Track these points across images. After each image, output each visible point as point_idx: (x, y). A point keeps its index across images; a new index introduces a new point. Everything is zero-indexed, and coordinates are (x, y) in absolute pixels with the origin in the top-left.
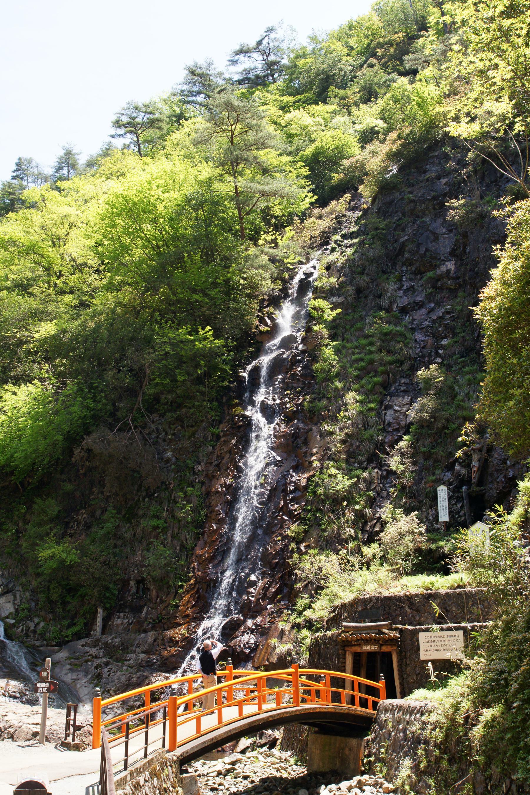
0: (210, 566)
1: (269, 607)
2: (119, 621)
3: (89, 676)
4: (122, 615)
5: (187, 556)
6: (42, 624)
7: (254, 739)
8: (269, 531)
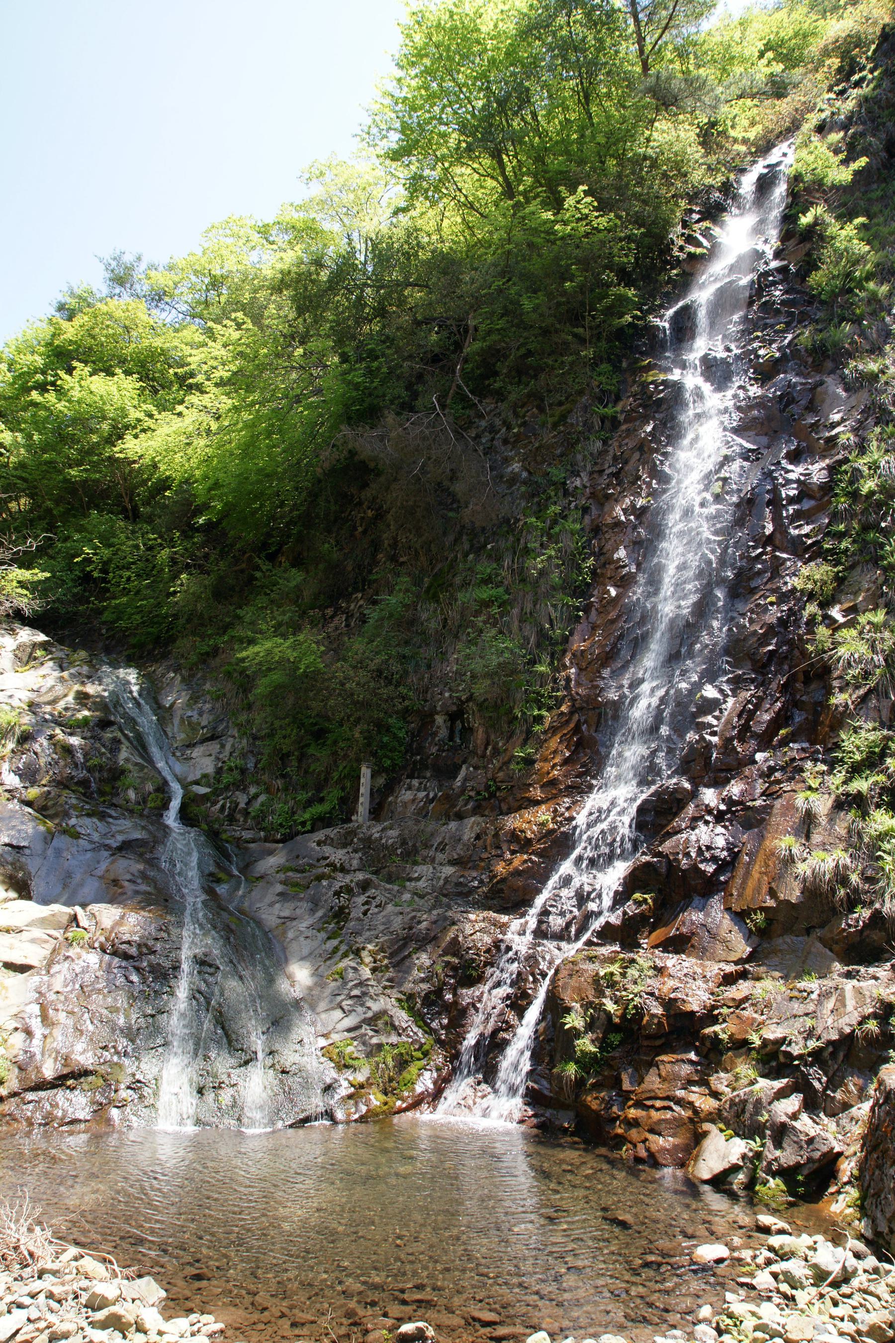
0: (606, 673)
1: (759, 756)
2: (407, 796)
3: (320, 913)
4: (415, 782)
5: (552, 656)
6: (262, 798)
7: (755, 1145)
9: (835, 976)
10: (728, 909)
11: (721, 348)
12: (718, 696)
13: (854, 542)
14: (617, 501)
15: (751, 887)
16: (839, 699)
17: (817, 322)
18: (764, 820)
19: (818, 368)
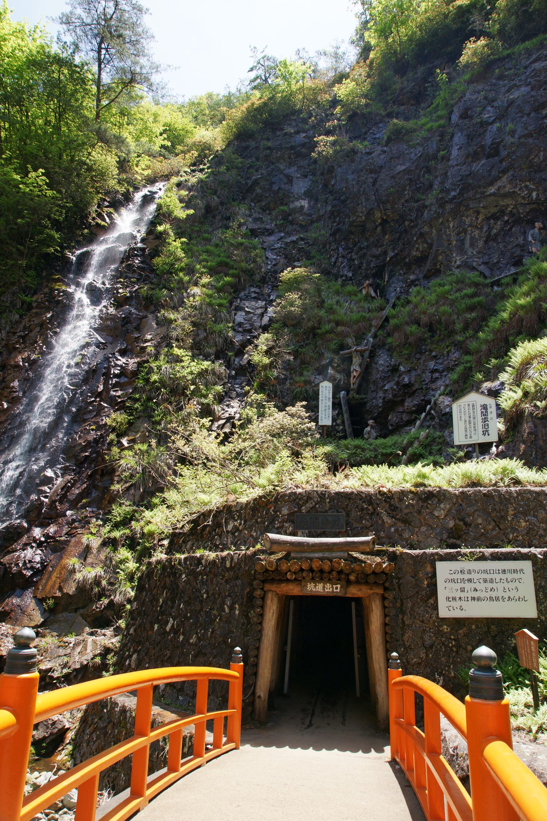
1: (69, 513)
8: (78, 419)
9: (85, 634)
10: (35, 597)
11: (100, 282)
12: (53, 476)
13: (142, 405)
14: (20, 352)
15: (50, 586)
16: (116, 487)
17: (152, 283)
18: (64, 548)
19: (146, 308)
